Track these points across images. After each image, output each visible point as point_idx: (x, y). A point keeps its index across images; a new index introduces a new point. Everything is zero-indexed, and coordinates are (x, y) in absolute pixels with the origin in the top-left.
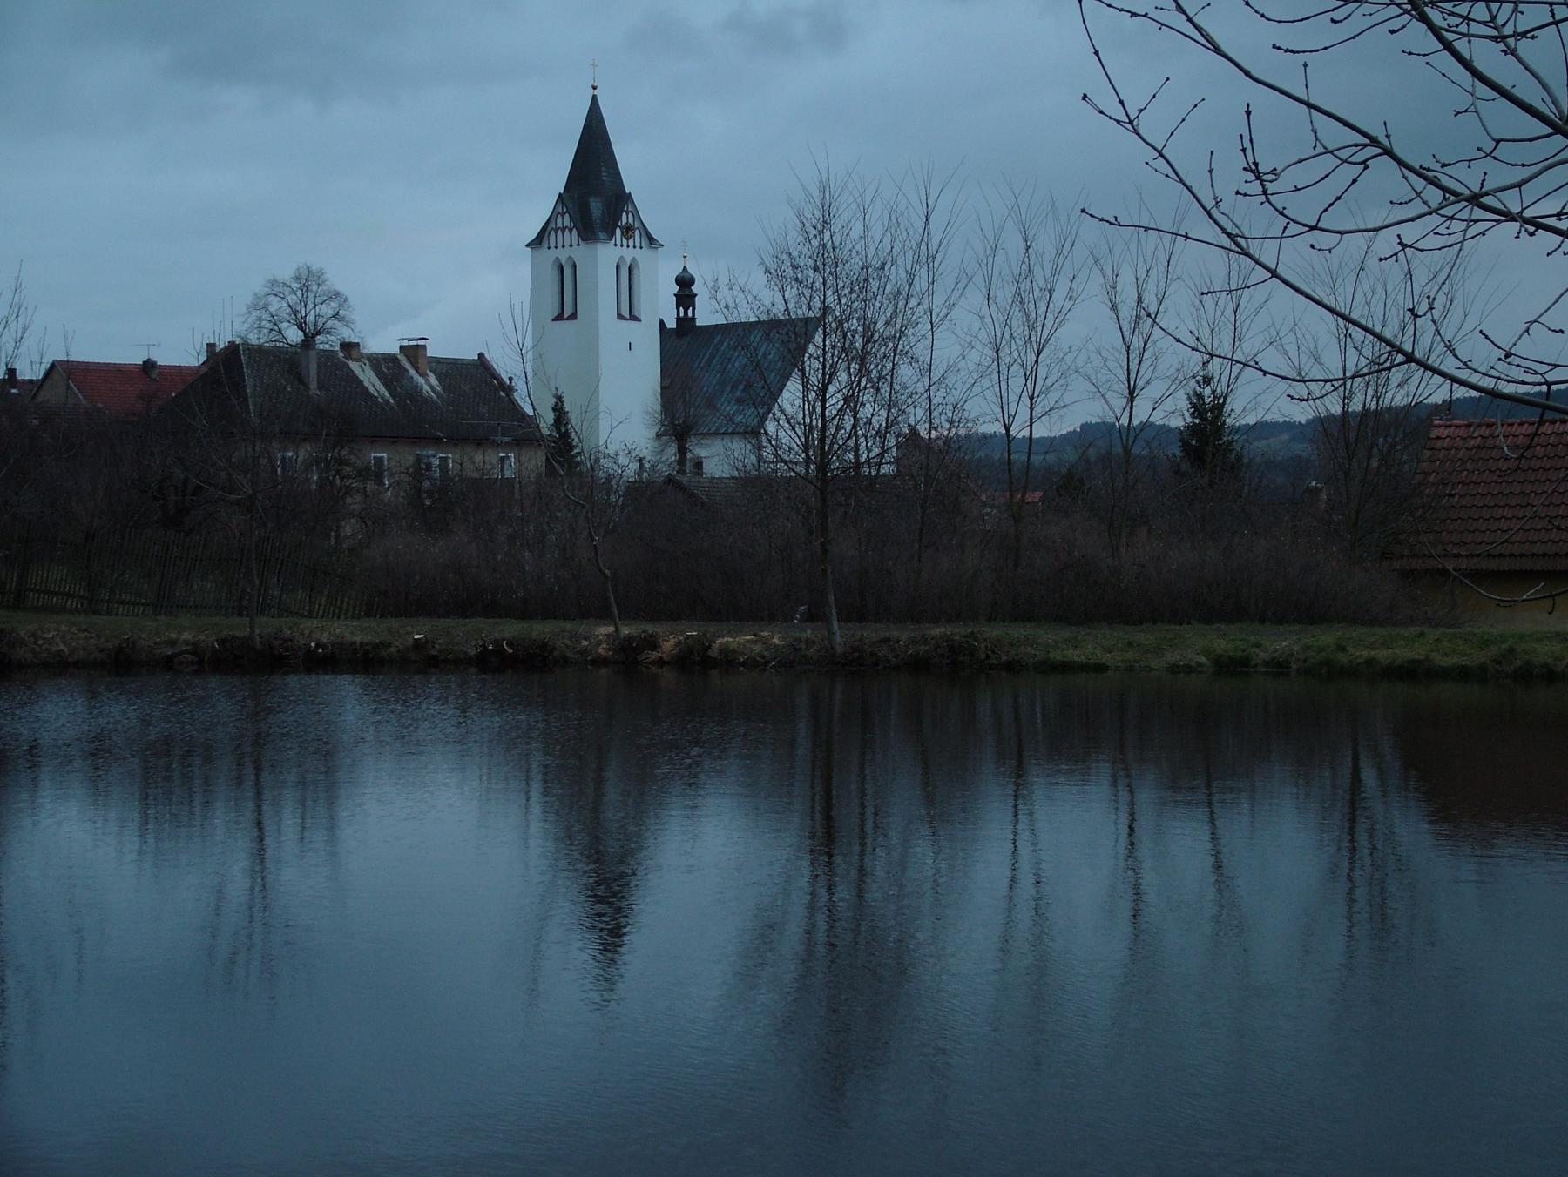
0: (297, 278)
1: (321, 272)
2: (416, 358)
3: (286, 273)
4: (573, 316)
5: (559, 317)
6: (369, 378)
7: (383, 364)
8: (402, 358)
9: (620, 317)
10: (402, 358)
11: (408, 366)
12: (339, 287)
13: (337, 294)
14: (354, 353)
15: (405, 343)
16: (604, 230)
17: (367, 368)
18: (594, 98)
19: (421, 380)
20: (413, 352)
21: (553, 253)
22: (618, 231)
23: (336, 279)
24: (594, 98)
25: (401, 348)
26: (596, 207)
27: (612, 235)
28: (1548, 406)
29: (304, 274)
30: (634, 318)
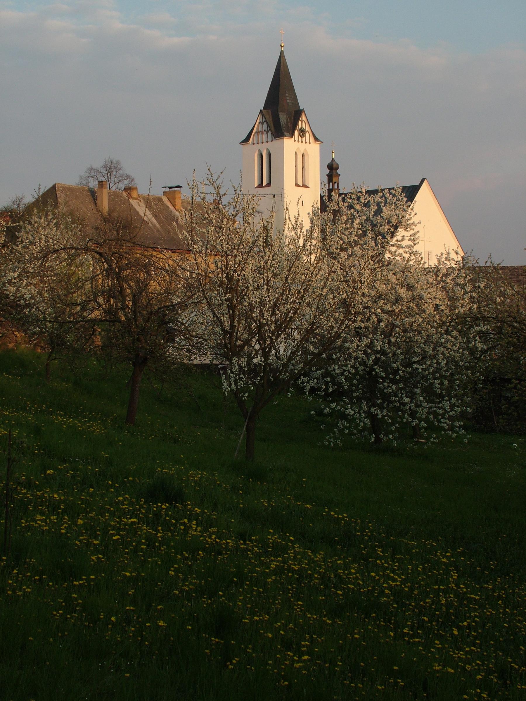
0: (105, 167)
1: (118, 163)
2: (174, 199)
3: (98, 164)
4: (269, 185)
5: (260, 185)
6: (141, 209)
7: (150, 202)
8: (165, 199)
9: (297, 185)
10: (165, 199)
11: (169, 204)
12: (128, 172)
13: (128, 177)
14: (134, 194)
15: (167, 189)
16: (288, 131)
17: (143, 204)
18: (282, 52)
19: (177, 213)
20: (172, 191)
21: (257, 147)
22: (296, 132)
23: (128, 168)
24: (282, 52)
25: (165, 193)
26: (283, 118)
27: (292, 135)
28: (516, 274)
29: (109, 164)
30: (304, 186)
